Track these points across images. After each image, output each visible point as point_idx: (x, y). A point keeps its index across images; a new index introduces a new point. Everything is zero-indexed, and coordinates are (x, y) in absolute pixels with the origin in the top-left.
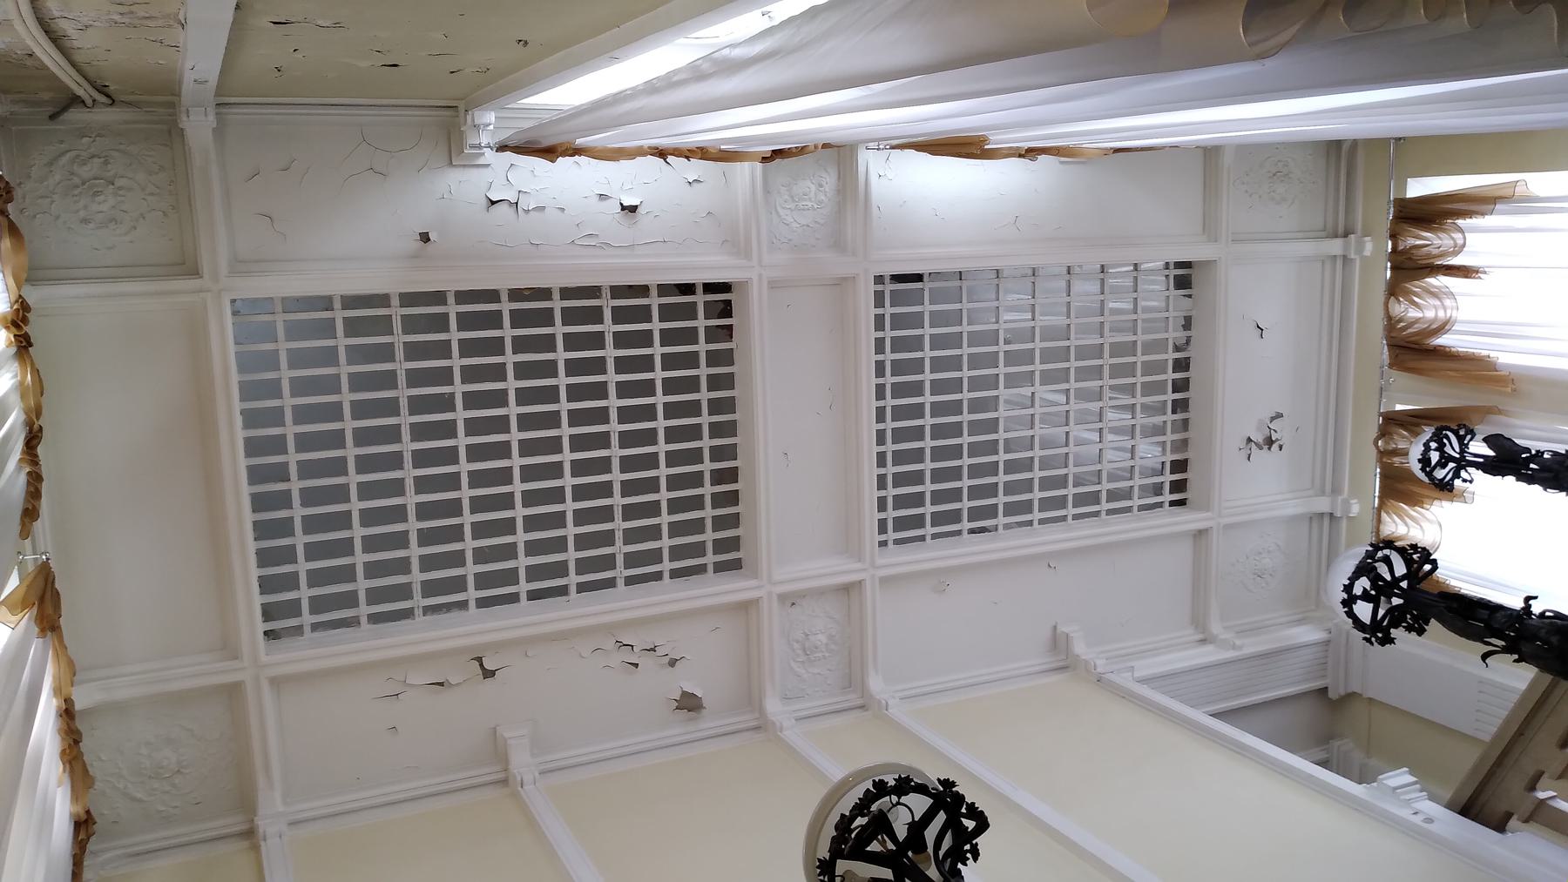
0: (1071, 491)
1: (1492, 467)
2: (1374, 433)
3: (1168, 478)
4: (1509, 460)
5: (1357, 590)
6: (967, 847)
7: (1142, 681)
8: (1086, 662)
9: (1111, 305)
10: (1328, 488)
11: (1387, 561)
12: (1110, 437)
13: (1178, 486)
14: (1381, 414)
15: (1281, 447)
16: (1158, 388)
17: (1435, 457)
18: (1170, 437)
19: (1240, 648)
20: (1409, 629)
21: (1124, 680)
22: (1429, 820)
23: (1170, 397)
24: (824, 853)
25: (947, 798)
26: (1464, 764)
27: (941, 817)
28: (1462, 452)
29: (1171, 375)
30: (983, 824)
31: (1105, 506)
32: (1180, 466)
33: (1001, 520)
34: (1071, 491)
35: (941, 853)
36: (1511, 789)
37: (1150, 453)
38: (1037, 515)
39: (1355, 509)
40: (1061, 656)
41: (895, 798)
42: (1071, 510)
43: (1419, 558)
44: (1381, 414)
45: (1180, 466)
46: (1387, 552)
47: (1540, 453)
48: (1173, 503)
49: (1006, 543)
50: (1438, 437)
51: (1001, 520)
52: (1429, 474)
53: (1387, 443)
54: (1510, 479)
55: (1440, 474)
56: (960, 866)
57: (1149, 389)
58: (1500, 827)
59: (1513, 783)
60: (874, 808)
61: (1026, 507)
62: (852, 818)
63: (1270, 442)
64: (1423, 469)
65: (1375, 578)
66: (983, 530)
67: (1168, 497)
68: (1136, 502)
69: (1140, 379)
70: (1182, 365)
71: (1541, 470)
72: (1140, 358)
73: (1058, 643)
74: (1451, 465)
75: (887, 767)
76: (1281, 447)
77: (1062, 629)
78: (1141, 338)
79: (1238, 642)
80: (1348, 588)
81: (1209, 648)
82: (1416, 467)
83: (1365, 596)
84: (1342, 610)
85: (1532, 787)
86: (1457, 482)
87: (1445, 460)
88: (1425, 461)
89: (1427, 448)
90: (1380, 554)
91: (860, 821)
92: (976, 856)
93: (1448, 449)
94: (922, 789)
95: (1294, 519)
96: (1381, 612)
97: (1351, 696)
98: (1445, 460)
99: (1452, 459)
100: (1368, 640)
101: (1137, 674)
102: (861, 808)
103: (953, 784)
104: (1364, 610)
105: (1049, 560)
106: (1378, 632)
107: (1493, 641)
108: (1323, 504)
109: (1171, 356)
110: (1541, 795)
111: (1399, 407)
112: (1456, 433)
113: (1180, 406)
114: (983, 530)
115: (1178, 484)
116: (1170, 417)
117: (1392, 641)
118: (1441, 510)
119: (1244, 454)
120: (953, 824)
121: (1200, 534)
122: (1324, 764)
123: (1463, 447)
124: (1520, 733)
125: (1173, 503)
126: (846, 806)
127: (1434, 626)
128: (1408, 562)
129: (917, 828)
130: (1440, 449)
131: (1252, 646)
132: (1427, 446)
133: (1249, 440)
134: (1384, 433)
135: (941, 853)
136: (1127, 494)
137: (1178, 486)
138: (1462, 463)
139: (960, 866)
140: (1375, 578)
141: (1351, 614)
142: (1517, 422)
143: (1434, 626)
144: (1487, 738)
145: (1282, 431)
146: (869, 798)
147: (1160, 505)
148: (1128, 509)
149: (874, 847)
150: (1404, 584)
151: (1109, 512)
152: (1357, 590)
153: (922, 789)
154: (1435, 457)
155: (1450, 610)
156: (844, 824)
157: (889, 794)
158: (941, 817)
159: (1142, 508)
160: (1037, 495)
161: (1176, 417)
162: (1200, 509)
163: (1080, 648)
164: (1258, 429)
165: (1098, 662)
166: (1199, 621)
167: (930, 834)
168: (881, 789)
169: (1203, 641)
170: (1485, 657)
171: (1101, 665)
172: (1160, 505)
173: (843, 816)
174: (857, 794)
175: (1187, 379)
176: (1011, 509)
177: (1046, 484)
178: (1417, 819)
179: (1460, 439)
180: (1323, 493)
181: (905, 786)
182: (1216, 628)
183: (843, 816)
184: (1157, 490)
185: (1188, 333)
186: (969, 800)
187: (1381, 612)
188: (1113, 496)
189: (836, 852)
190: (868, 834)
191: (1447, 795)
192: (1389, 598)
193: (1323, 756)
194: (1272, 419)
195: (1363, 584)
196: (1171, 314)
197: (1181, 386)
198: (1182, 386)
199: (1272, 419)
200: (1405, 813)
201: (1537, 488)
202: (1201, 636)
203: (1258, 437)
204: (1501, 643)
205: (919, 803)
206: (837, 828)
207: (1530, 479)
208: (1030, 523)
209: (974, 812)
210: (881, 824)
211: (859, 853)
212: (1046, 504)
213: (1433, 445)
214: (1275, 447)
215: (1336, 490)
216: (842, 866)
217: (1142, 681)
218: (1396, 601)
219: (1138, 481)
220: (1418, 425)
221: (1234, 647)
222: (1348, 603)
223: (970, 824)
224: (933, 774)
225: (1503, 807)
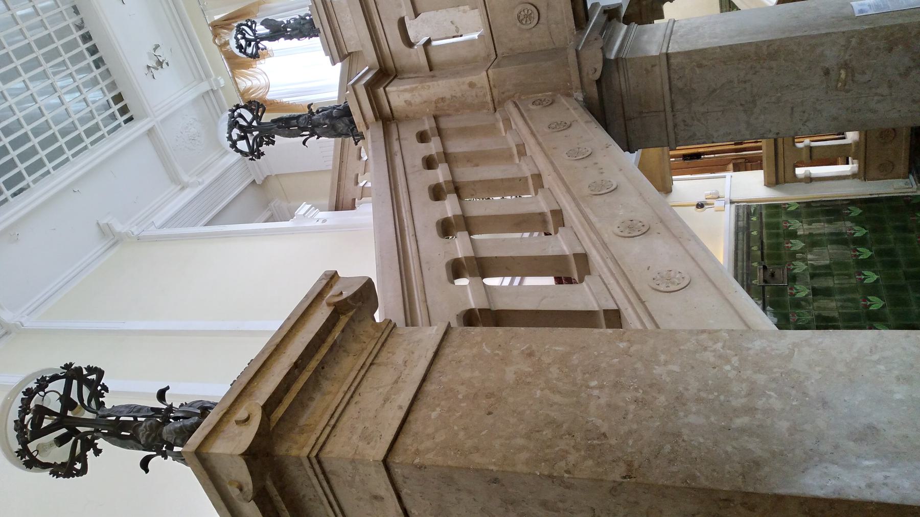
0: (62, 142)
1: (272, 37)
2: (211, 37)
3: (115, 108)
4: (277, 31)
5: (235, 137)
6: (99, 388)
7: (162, 227)
8: (126, 234)
9: (19, 13)
10: (203, 76)
11: (241, 116)
12: (78, 77)
13: (124, 110)
14: (209, 25)
15: (167, 64)
16: (78, 58)
17: (243, 42)
18: (103, 84)
19: (203, 182)
20: (268, 144)
21: (153, 231)
22: (324, 221)
23: (90, 59)
24: (17, 447)
25: (71, 373)
26: (327, 183)
27: (75, 382)
28: (255, 34)
29: (83, 47)
30: (100, 373)
31: (87, 141)
32: (118, 98)
33: (29, 179)
34: (62, 142)
35: (86, 402)
36: (350, 190)
37: (97, 96)
38: (49, 166)
39: (222, 82)
40: (110, 237)
41: (42, 393)
42: (69, 153)
43: (256, 106)
44: (209, 25)
45: (118, 98)
46: (238, 111)
47: (289, 22)
48: (126, 122)
49: (39, 192)
50: (240, 31)
51: (29, 179)
52: (245, 53)
53: (220, 40)
54: (282, 40)
55: (249, 50)
56: (101, 399)
57: (76, 59)
58: (353, 207)
59: (349, 184)
60: (32, 405)
61: (40, 164)
62: (22, 420)
63: (160, 63)
64: (241, 51)
65: (241, 128)
66: (21, 190)
67: (121, 119)
68: (105, 130)
69: (66, 56)
70: (87, 38)
71: (293, 30)
72: (59, 43)
73: (105, 231)
74: (253, 43)
75: (27, 380)
76: (167, 64)
77: (103, 222)
78: (51, 30)
79: (200, 180)
80: (230, 138)
81: (187, 191)
82: (237, 51)
83: (241, 138)
84: (232, 150)
85: (357, 183)
86: (260, 51)
87: (249, 42)
88: (240, 47)
89: (237, 40)
90: (236, 114)
91: (28, 417)
92: (106, 390)
93: (247, 36)
94: (55, 378)
95: (195, 101)
96: (251, 142)
97: (267, 178)
98: (249, 42)
99: (253, 40)
100: (252, 159)
101: (158, 224)
102: (24, 410)
103: (71, 364)
104: (242, 145)
105: (72, 188)
106: (255, 153)
107: (304, 133)
108: (205, 87)
109: (77, 34)
110: (361, 184)
111: (217, 18)
112: (247, 25)
113: (99, 63)
114: (21, 190)
115: (122, 108)
116: (97, 72)
117: (263, 154)
118: (262, 65)
119: (150, 75)
120: (83, 381)
121: (150, 132)
122: (271, 219)
123: (254, 31)
124: (341, 162)
125: (126, 122)
126: (14, 415)
127: (277, 138)
128: (251, 111)
129: (66, 400)
130: (244, 38)
131: (208, 178)
132: (236, 38)
133: (148, 67)
134: (216, 36)
135: (86, 402)
136: (96, 128)
137: (124, 110)
138: (258, 39)
139: (101, 399)
140: (241, 128)
141: (238, 150)
142: (271, 5)
143: (277, 138)
144: (330, 168)
145: (163, 54)
146: (25, 403)
147: (119, 126)
148: (103, 137)
149: (46, 422)
150: (255, 123)
151: (92, 143)
152: (235, 137)
153: (55, 378)
154: (243, 42)
155: (279, 127)
156: (20, 425)
157: (37, 392)
158: (75, 382)
159: (109, 132)
160: (42, 154)
161: (100, 70)
162: (142, 118)
163: (119, 228)
164: (150, 58)
165: (133, 230)
166: (174, 179)
167: (74, 396)
168: (30, 394)
169: (183, 189)
170: (304, 143)
171: (135, 230)
172: (119, 126)
173: (15, 421)
174: (17, 403)
175: (94, 45)
176: (31, 170)
177: (44, 144)
178: (320, 223)
179: (250, 27)
180: (202, 80)
181: (43, 384)
182: (185, 178)
183: (15, 421)
184: (113, 117)
185: (80, 17)
186: (84, 366)
187: (251, 142)
188: (89, 133)
189: (24, 442)
190: (37, 423)
191: (326, 202)
192: (251, 133)
193: (267, 214)
194: (155, 50)
195: (236, 132)
196: (63, 8)
197: (93, 50)
198: (93, 51)
199: (155, 50)
200: (313, 224)
201: (295, 40)
202: (180, 187)
203: (153, 63)
204: (308, 133)
205: (59, 386)
206: (16, 430)
207: (290, 37)
208: (48, 172)
209: (91, 370)
210: (42, 411)
211: (38, 432)
212: (51, 157)
213: (239, 36)
214: (164, 65)
215: (208, 76)
216: (32, 446)
217: (162, 227)
218: (255, 133)
219: (98, 119)
220: (230, 24)
221: (200, 184)
222: (234, 145)
223: (94, 377)
224: (56, 364)
225: (350, 198)
